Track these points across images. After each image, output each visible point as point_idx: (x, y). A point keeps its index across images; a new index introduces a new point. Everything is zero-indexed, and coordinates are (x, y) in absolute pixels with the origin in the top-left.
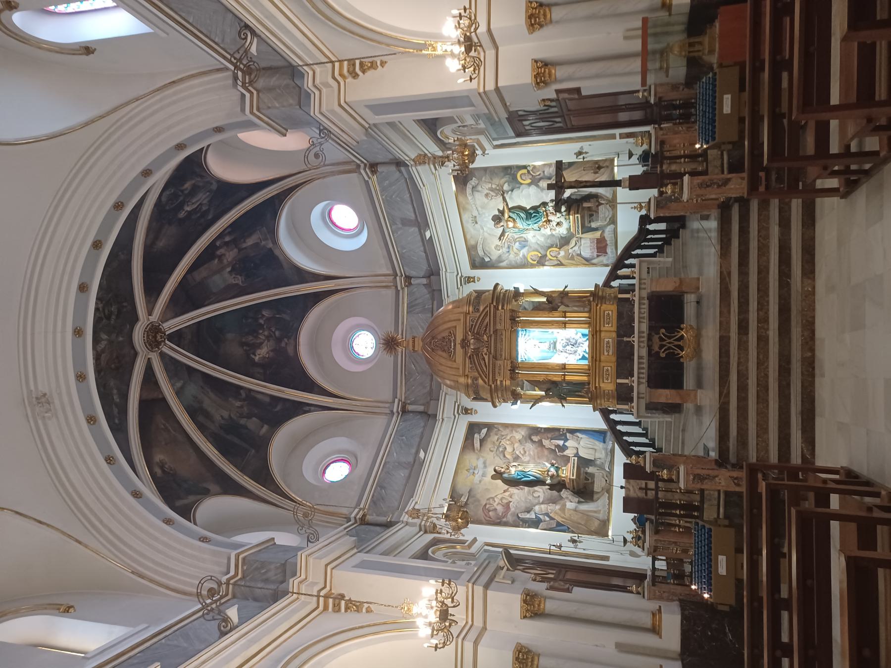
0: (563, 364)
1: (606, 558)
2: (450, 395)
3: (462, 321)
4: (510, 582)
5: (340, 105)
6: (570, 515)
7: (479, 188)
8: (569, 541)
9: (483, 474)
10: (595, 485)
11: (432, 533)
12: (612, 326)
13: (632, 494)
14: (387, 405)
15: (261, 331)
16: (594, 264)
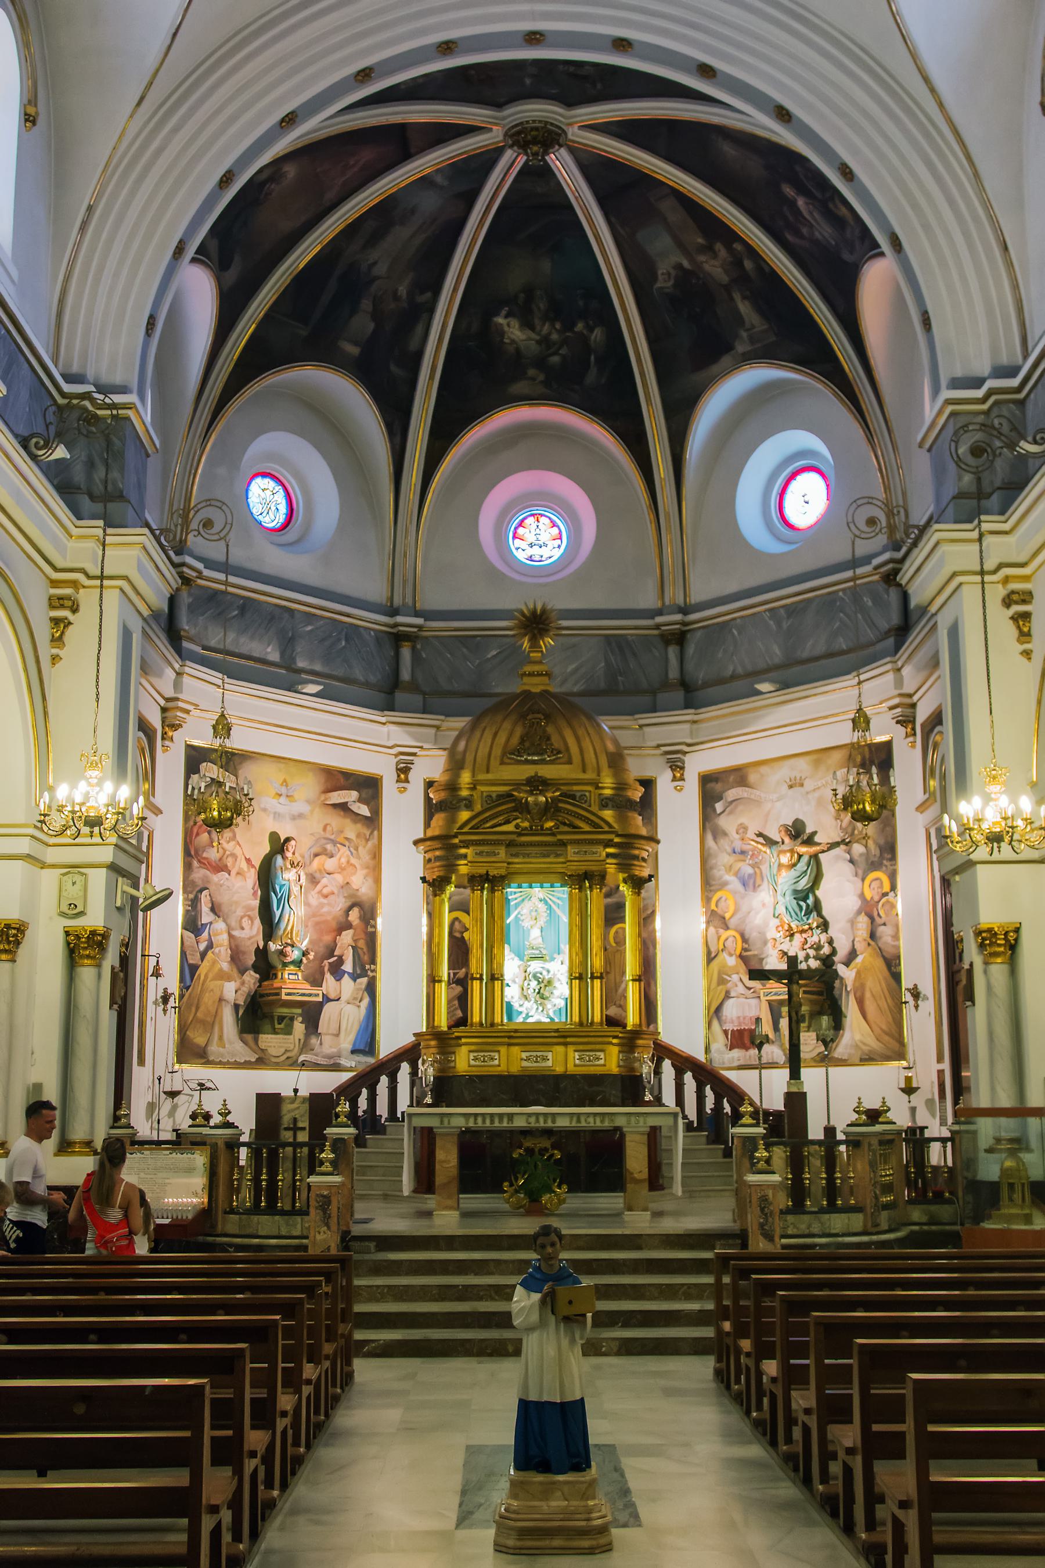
0: (502, 976)
1: (142, 1062)
2: (436, 735)
3: (582, 776)
4: (118, 904)
5: (954, 574)
6: (212, 990)
8: (165, 990)
9: (279, 814)
11: (163, 722)
12: (575, 1065)
13: (286, 1107)
15: (558, 326)
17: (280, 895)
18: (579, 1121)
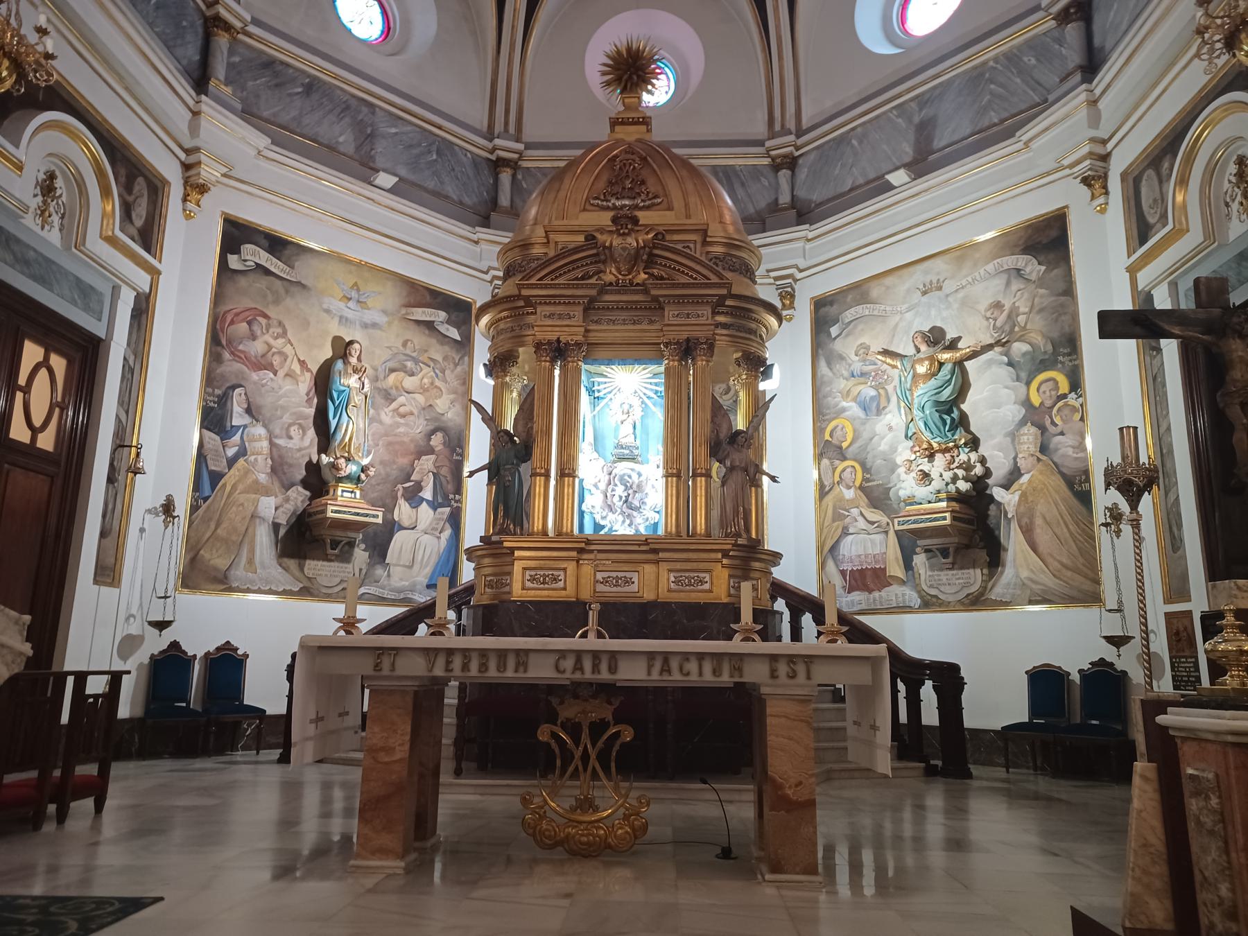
0: (574, 472)
1: (108, 573)
6: (242, 505)
7: (1016, 285)
9: (347, 319)
10: (320, 563)
12: (669, 590)
14: (512, 129)
16: (822, 565)
17: (337, 403)
18: (666, 669)
